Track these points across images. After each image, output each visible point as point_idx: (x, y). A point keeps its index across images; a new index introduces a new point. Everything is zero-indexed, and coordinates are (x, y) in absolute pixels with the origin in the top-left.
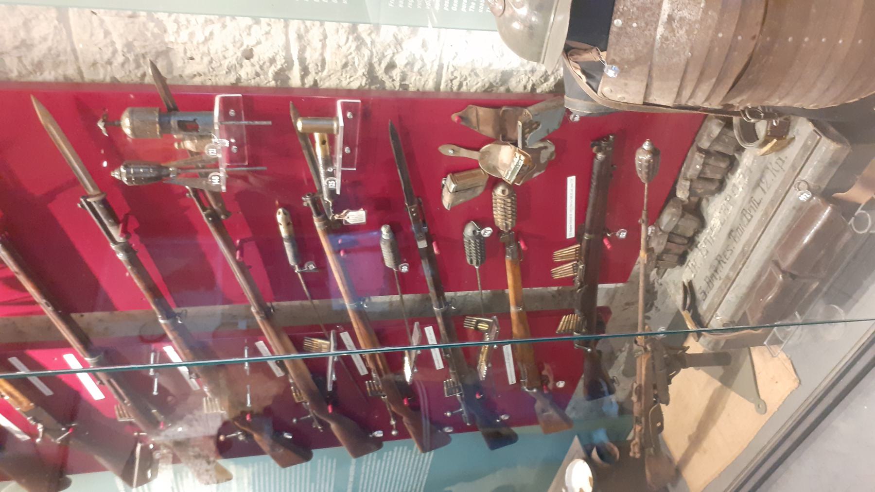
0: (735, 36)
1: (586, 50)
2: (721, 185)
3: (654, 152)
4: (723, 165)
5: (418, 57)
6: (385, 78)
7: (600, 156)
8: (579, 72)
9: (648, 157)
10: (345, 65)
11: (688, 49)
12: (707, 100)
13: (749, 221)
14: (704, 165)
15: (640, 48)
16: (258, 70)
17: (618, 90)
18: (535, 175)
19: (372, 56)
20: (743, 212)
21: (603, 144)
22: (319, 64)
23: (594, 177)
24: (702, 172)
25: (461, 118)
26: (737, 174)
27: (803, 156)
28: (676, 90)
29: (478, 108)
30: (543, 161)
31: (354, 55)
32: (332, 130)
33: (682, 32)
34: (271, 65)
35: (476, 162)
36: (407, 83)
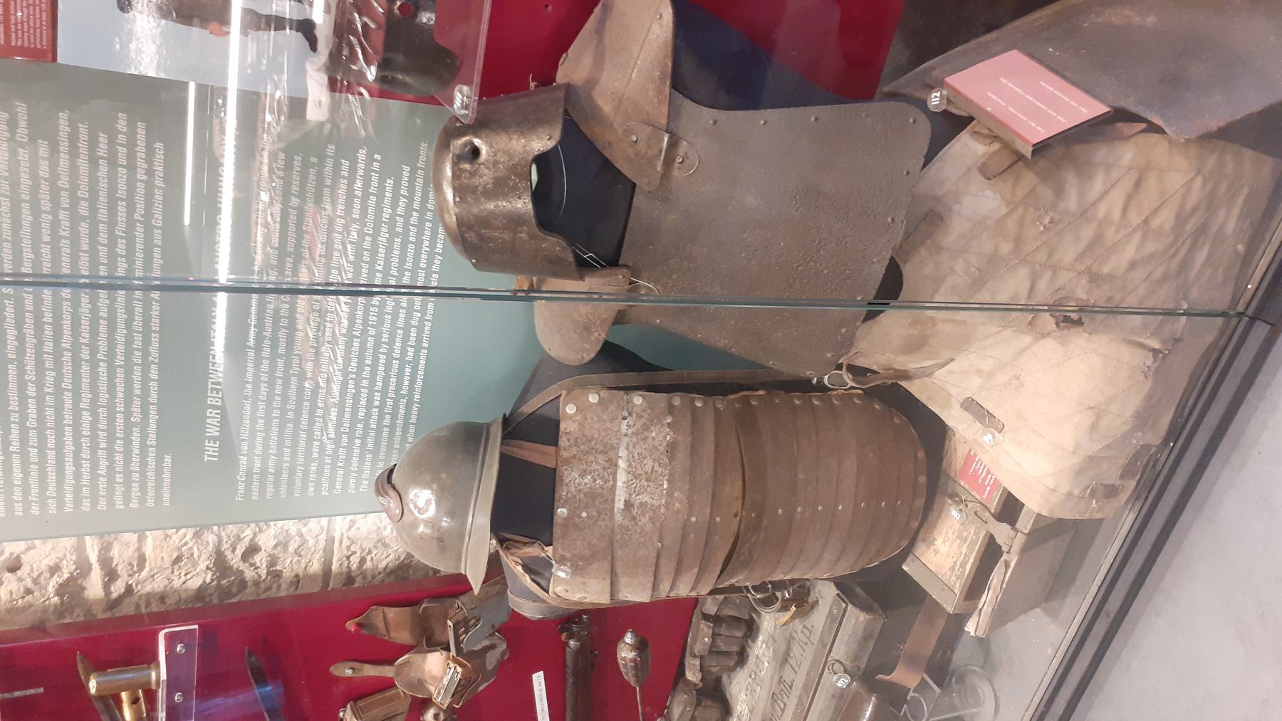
0: (712, 517)
1: (525, 544)
2: (742, 658)
3: (640, 647)
4: (739, 634)
5: (293, 532)
6: (242, 566)
7: (572, 643)
8: (520, 568)
9: (631, 655)
10: (178, 560)
11: (655, 539)
12: (692, 589)
13: (783, 710)
14: (714, 635)
15: (594, 541)
16: (29, 583)
17: (573, 587)
18: (481, 688)
19: (220, 542)
20: (774, 697)
21: (575, 628)
22: (135, 563)
23: (569, 671)
24: (713, 644)
25: (359, 625)
26: (759, 643)
27: (830, 629)
28: (650, 585)
29: (386, 609)
30: (490, 667)
31: (190, 545)
32: (149, 683)
33: (645, 520)
34: (52, 575)
35: (391, 680)
36: (278, 568)
